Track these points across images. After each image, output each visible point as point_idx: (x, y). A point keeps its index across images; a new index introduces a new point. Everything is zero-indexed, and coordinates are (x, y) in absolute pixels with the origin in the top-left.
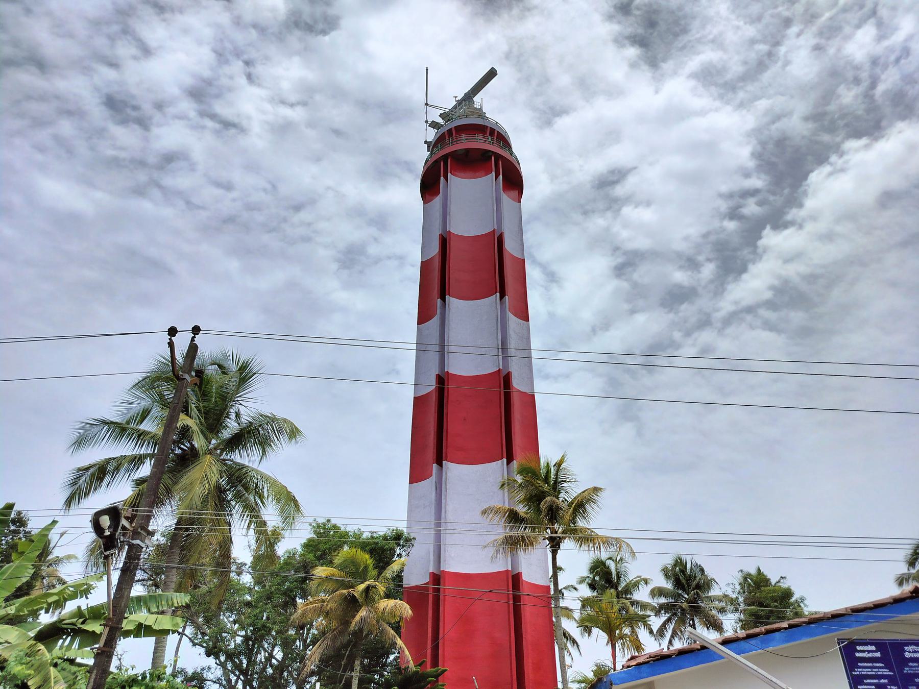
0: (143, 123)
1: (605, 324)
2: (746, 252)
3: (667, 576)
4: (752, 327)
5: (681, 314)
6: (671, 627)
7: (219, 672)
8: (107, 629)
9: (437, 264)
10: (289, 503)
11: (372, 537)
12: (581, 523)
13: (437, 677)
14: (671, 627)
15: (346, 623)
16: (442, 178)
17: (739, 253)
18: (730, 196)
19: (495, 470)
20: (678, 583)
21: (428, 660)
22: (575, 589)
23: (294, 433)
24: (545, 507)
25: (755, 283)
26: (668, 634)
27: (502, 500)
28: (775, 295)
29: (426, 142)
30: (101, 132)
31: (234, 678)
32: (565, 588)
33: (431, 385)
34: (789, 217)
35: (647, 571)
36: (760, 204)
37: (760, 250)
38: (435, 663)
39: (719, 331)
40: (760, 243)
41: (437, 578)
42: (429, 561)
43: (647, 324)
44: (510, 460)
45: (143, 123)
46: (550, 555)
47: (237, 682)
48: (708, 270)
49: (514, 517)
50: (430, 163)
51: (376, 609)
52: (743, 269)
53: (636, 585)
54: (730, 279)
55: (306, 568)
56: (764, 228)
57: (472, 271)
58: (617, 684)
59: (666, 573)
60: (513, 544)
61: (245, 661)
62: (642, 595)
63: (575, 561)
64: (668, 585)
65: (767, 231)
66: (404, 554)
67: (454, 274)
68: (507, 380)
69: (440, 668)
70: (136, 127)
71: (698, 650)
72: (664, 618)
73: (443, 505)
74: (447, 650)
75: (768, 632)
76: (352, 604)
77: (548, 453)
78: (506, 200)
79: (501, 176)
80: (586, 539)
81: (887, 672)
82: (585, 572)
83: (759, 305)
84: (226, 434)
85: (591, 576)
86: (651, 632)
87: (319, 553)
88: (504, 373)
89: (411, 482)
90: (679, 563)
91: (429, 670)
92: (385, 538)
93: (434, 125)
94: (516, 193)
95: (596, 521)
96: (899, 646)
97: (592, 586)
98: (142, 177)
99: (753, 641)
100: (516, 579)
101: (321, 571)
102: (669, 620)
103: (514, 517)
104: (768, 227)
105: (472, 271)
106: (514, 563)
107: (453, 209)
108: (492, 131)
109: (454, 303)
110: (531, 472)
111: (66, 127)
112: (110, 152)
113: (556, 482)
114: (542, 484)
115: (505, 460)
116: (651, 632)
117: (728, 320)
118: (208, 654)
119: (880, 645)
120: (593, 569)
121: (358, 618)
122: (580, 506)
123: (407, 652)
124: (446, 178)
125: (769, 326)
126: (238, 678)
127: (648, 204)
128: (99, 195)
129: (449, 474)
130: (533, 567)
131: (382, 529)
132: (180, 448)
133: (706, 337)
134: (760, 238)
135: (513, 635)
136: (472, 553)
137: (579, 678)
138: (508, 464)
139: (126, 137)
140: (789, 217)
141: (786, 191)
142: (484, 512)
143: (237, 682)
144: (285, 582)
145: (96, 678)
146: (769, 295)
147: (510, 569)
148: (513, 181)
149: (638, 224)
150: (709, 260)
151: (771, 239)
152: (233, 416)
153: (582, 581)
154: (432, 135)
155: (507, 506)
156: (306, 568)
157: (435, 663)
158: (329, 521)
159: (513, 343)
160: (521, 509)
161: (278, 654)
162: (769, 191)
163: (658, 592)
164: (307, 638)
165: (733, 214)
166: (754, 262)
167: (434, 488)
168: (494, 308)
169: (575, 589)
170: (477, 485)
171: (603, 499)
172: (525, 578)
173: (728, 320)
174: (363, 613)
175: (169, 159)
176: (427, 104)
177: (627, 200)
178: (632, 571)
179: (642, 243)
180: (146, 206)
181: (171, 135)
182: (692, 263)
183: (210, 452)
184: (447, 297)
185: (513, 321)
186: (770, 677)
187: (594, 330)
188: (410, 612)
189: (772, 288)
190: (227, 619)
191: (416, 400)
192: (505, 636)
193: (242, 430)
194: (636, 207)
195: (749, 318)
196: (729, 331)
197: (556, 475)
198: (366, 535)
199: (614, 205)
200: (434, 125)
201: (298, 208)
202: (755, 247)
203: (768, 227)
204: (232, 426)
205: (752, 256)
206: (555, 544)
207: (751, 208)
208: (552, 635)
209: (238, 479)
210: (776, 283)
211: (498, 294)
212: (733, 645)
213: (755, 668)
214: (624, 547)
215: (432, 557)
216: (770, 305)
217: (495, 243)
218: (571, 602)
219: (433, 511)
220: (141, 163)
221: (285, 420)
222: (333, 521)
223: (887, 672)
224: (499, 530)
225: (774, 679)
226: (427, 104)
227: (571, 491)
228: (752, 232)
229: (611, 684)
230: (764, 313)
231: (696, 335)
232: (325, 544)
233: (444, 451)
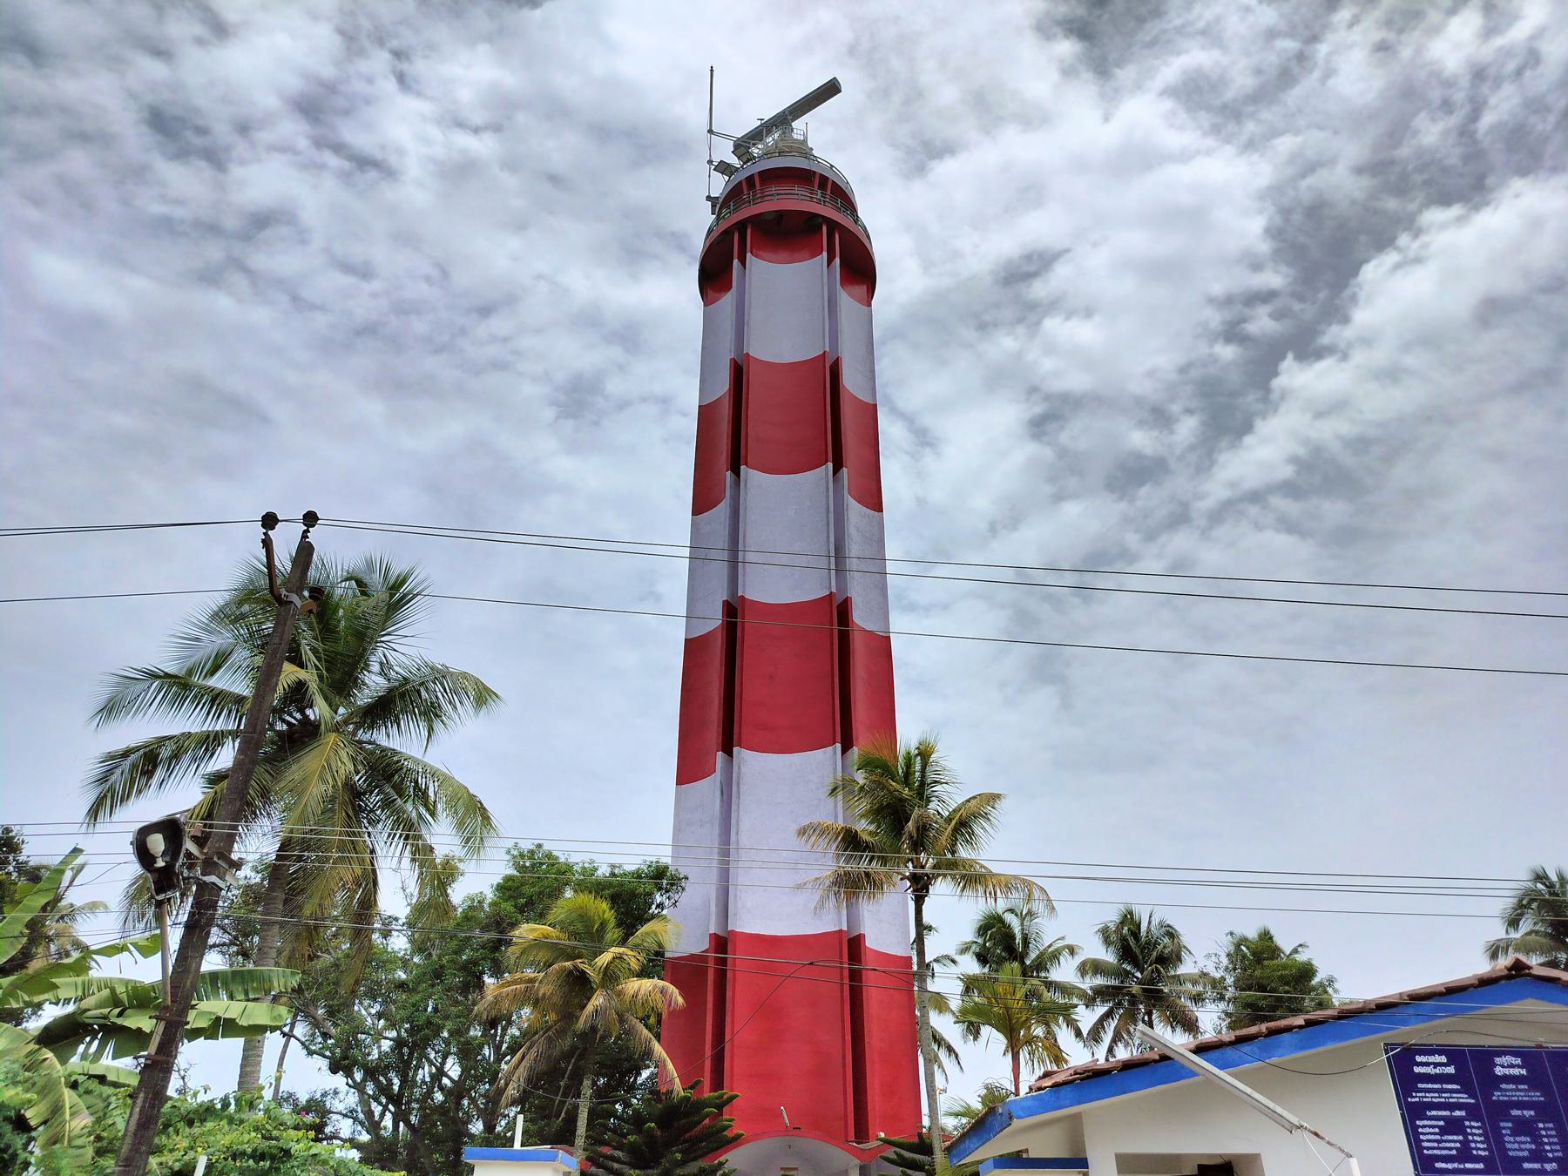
0: (216, 159)
1: (1011, 517)
2: (1251, 399)
3: (1107, 941)
4: (1259, 527)
5: (1139, 504)
6: (1111, 1026)
7: (352, 1099)
8: (162, 1024)
9: (726, 412)
10: (474, 816)
11: (613, 875)
12: (964, 852)
13: (720, 1107)
14: (1111, 1026)
15: (568, 1015)
16: (736, 262)
17: (1240, 400)
18: (1228, 301)
19: (822, 763)
20: (1126, 953)
21: (706, 1080)
22: (954, 961)
23: (483, 696)
24: (902, 825)
25: (1264, 453)
26: (1107, 1038)
27: (833, 813)
28: (1298, 473)
29: (709, 198)
30: (140, 173)
31: (377, 1109)
32: (937, 960)
33: (714, 620)
34: (1325, 340)
35: (1074, 933)
36: (1277, 316)
37: (1275, 396)
38: (718, 1083)
39: (1203, 532)
40: (1276, 383)
41: (721, 943)
42: (709, 915)
43: (1083, 520)
44: (846, 749)
45: (216, 159)
46: (912, 905)
47: (382, 1115)
48: (1187, 428)
49: (851, 841)
50: (715, 234)
51: (620, 994)
52: (1247, 428)
53: (1055, 956)
54: (1224, 444)
55: (500, 925)
56: (1283, 358)
57: (787, 424)
58: (1019, 1117)
59: (1105, 933)
60: (851, 886)
61: (396, 1081)
62: (1065, 972)
63: (954, 916)
64: (1109, 957)
65: (1288, 363)
66: (667, 903)
67: (757, 428)
68: (843, 610)
69: (727, 1092)
70: (203, 164)
71: (1155, 1061)
72: (1101, 1010)
73: (733, 822)
74: (736, 1064)
75: (1272, 1033)
76: (579, 985)
77: (908, 735)
78: (847, 301)
79: (837, 260)
80: (972, 878)
81: (1464, 1098)
82: (969, 935)
83: (1271, 489)
84: (363, 698)
85: (980, 941)
86: (1078, 1033)
87: (522, 901)
88: (839, 599)
89: (681, 780)
90: (1129, 919)
91: (707, 1094)
92: (638, 875)
93: (723, 168)
94: (861, 290)
95: (991, 849)
96: (1485, 1057)
97: (982, 958)
98: (214, 252)
99: (1246, 1048)
100: (854, 945)
101: (527, 931)
102: (1108, 1015)
103: (851, 841)
104: (1290, 356)
105: (787, 424)
106: (852, 918)
107: (755, 315)
108: (824, 180)
109: (751, 476)
110: (880, 767)
111: (78, 162)
112: (157, 208)
113: (923, 783)
114: (898, 787)
115: (839, 746)
116: (1078, 1033)
117: (1218, 516)
118: (334, 1070)
119: (1454, 1054)
120: (983, 930)
121: (590, 1008)
122: (963, 825)
123: (670, 1066)
124: (743, 262)
125: (1289, 526)
126: (385, 1108)
127: (1088, 313)
128: (138, 283)
129: (743, 769)
130: (884, 924)
131: (632, 861)
132: (284, 721)
133: (1181, 542)
134: (1276, 374)
135: (849, 1037)
136: (782, 900)
137: (957, 1108)
138: (844, 751)
139: (184, 183)
140: (1325, 340)
141: (1322, 295)
142: (802, 832)
143: (382, 1115)
144: (465, 949)
145: (143, 1108)
146: (1287, 472)
147: (845, 928)
148: (858, 268)
149: (1072, 346)
150: (1189, 411)
151: (1295, 377)
152: (375, 667)
153: (964, 950)
154: (719, 185)
155: (841, 823)
156: (500, 925)
157: (718, 1083)
158: (540, 846)
159: (854, 548)
160: (863, 827)
161: (453, 1069)
162: (1293, 295)
163: (1095, 967)
164: (501, 1042)
165: (1232, 333)
166: (1264, 415)
167: (718, 793)
168: (823, 489)
169: (954, 961)
170: (792, 792)
171: (1002, 813)
172: (870, 943)
173: (1218, 516)
174: (598, 1000)
175: (261, 222)
176: (710, 131)
177: (1052, 306)
178: (1048, 932)
179: (1077, 381)
180: (222, 303)
181: (262, 180)
182: (1159, 417)
183: (337, 728)
184: (736, 749)
185: (855, 511)
186: (1271, 1105)
187: (993, 529)
188: (680, 1000)
189: (1294, 460)
190: (366, 1011)
191: (689, 644)
192: (836, 1041)
193: (391, 690)
194: (1067, 318)
195: (1253, 510)
196: (1221, 532)
197: (923, 771)
198: (603, 871)
199: (1030, 314)
200: (723, 168)
201: (485, 311)
202: (1268, 390)
203: (1290, 356)
204: (373, 683)
205: (1260, 406)
206: (921, 886)
207: (1262, 323)
208: (913, 1039)
209: (387, 772)
210: (1301, 451)
211: (830, 465)
212: (1215, 1054)
213: (1249, 1090)
214: (1036, 894)
215: (713, 908)
216: (1290, 489)
217: (827, 373)
218: (947, 983)
219: (716, 831)
220: (212, 229)
221: (465, 675)
222: (547, 847)
223: (1464, 1098)
224: (827, 862)
225: (1279, 1110)
226: (710, 131)
227: (948, 798)
228: (1263, 364)
229: (1011, 1118)
230: (1279, 502)
231: (1163, 538)
232: (535, 884)
233: (736, 730)
